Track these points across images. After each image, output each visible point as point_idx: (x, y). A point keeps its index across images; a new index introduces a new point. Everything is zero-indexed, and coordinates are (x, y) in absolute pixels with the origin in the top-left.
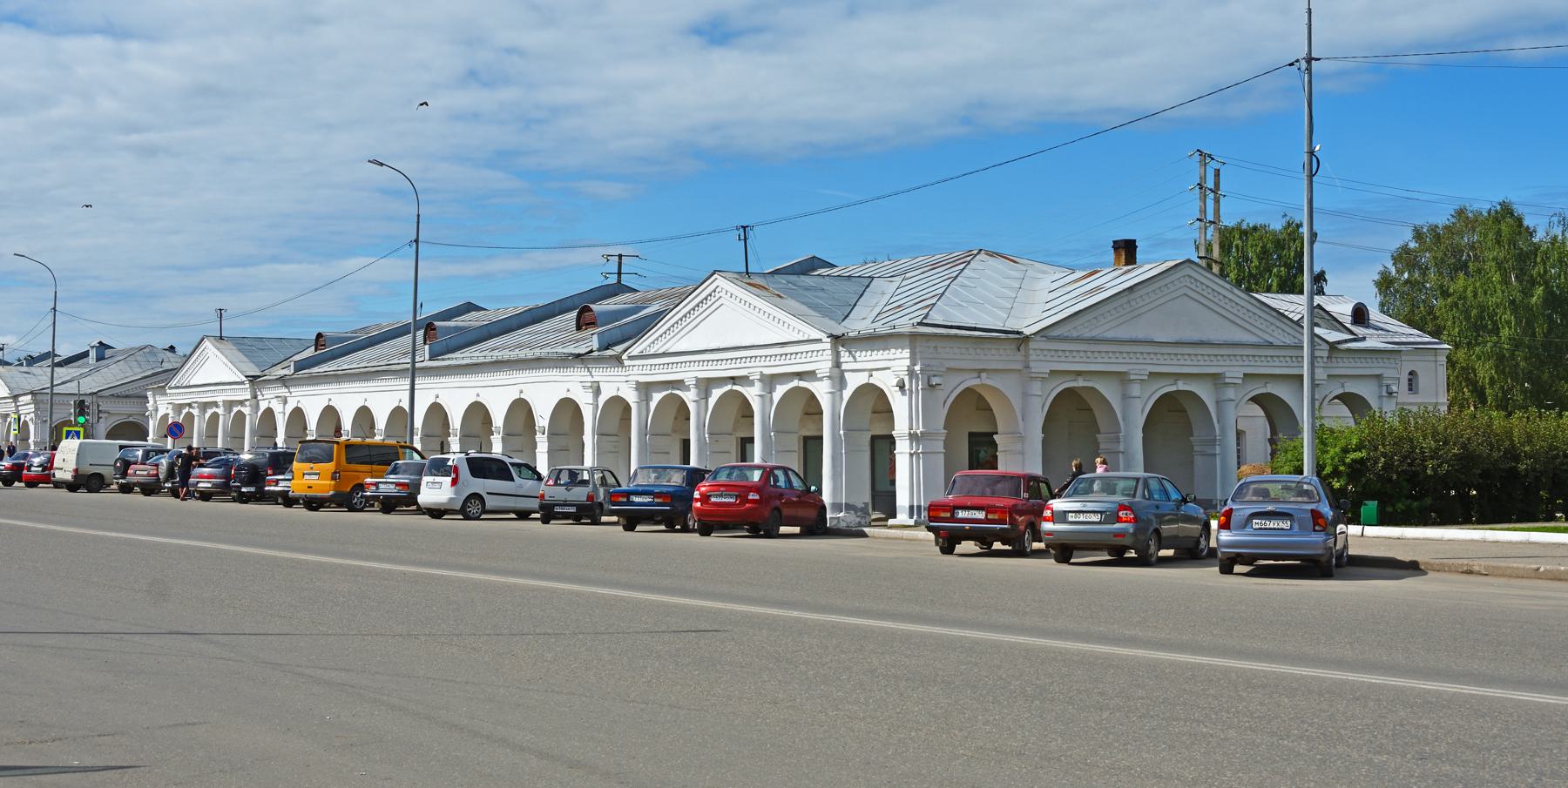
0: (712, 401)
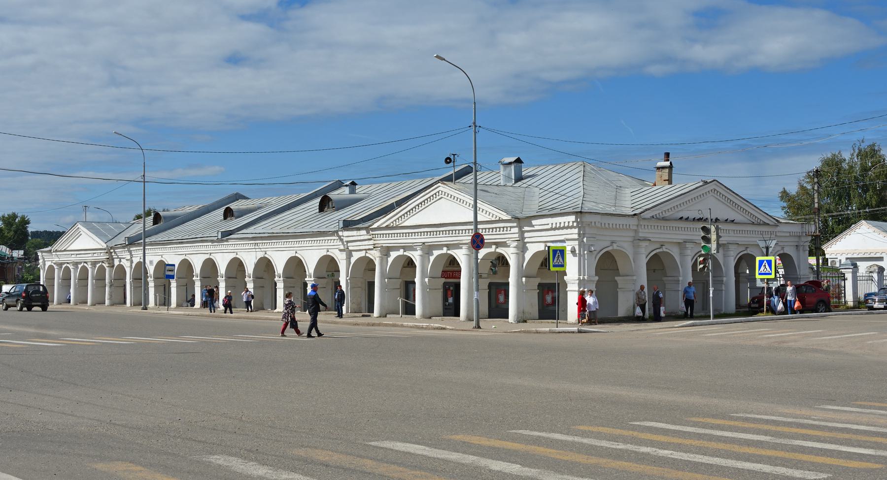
0: (390, 260)
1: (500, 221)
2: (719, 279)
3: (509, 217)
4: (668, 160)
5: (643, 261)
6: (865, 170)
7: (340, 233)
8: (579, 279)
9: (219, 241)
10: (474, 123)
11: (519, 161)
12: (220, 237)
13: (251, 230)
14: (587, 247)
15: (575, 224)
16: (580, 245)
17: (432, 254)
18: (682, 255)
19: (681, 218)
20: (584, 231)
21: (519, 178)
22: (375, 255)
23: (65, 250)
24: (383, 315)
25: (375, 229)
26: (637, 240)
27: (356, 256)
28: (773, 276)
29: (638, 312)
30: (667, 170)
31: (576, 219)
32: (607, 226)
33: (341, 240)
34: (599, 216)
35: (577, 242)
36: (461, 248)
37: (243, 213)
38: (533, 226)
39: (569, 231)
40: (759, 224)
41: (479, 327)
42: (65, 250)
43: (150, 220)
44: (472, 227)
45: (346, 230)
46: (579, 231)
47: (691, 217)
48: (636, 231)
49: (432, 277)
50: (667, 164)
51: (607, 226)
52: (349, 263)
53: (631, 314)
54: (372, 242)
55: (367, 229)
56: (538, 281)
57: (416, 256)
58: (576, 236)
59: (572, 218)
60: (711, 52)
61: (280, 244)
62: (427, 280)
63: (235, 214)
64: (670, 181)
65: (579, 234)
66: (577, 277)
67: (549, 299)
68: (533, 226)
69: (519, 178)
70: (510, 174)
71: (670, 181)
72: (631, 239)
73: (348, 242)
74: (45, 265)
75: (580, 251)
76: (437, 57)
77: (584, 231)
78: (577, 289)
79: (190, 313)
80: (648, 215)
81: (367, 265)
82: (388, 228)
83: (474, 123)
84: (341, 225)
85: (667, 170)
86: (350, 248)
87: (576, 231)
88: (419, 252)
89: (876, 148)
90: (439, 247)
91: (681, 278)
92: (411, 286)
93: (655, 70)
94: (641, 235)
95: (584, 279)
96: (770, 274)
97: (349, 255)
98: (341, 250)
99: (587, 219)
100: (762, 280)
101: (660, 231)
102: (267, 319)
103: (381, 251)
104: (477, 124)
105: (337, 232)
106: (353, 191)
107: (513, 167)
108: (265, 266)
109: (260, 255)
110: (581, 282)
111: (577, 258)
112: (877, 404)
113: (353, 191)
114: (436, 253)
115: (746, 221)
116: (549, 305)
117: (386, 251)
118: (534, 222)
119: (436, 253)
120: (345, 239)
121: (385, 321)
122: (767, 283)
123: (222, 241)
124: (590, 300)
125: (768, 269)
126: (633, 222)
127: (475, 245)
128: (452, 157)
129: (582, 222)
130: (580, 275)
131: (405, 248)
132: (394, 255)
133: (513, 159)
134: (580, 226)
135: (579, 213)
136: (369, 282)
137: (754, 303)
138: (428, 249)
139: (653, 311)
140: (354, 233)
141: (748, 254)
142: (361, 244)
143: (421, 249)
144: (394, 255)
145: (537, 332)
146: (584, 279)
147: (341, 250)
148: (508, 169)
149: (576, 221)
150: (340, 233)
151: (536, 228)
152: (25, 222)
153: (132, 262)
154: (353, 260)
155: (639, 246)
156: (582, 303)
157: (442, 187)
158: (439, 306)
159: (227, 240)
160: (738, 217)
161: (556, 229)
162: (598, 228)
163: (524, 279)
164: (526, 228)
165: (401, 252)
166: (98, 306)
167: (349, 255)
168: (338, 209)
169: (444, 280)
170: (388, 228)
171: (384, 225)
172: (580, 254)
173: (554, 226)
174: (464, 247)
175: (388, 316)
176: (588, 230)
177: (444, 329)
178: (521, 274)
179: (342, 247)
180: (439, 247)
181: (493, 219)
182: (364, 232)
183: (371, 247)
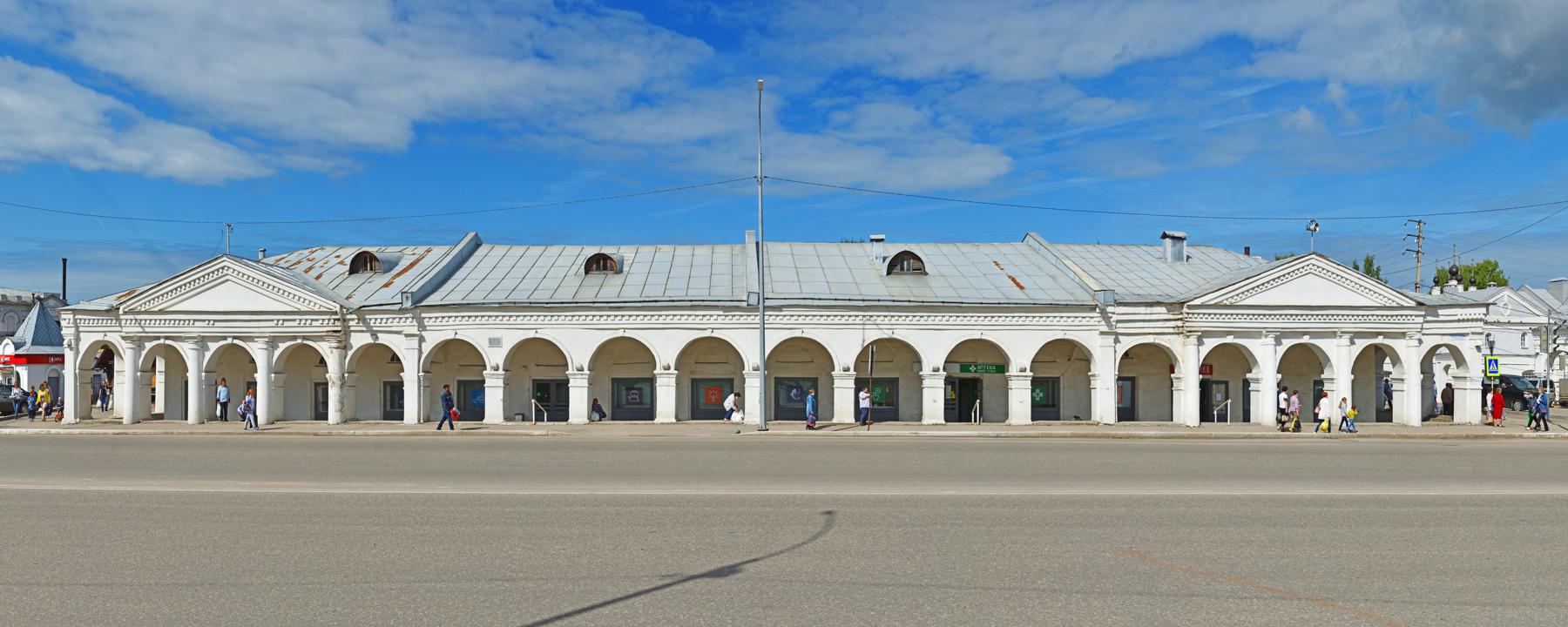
1: (1402, 308)
23: (161, 312)
25: (1190, 307)
27: (1127, 343)
42: (161, 312)
43: (941, 119)
57: (257, 351)
61: (581, 317)
74: (78, 339)
76: (65, 261)
82: (1216, 306)
92: (279, 412)
93: (87, 164)
98: (1102, 333)
116: (550, 399)
118: (1440, 312)
121: (352, 430)
131: (305, 338)
136: (317, 385)
138: (202, 342)
147: (1102, 333)
150: (1110, 309)
152: (1496, 265)
153: (345, 347)
165: (229, 341)
170: (1216, 306)
178: (270, 370)
179: (1106, 329)
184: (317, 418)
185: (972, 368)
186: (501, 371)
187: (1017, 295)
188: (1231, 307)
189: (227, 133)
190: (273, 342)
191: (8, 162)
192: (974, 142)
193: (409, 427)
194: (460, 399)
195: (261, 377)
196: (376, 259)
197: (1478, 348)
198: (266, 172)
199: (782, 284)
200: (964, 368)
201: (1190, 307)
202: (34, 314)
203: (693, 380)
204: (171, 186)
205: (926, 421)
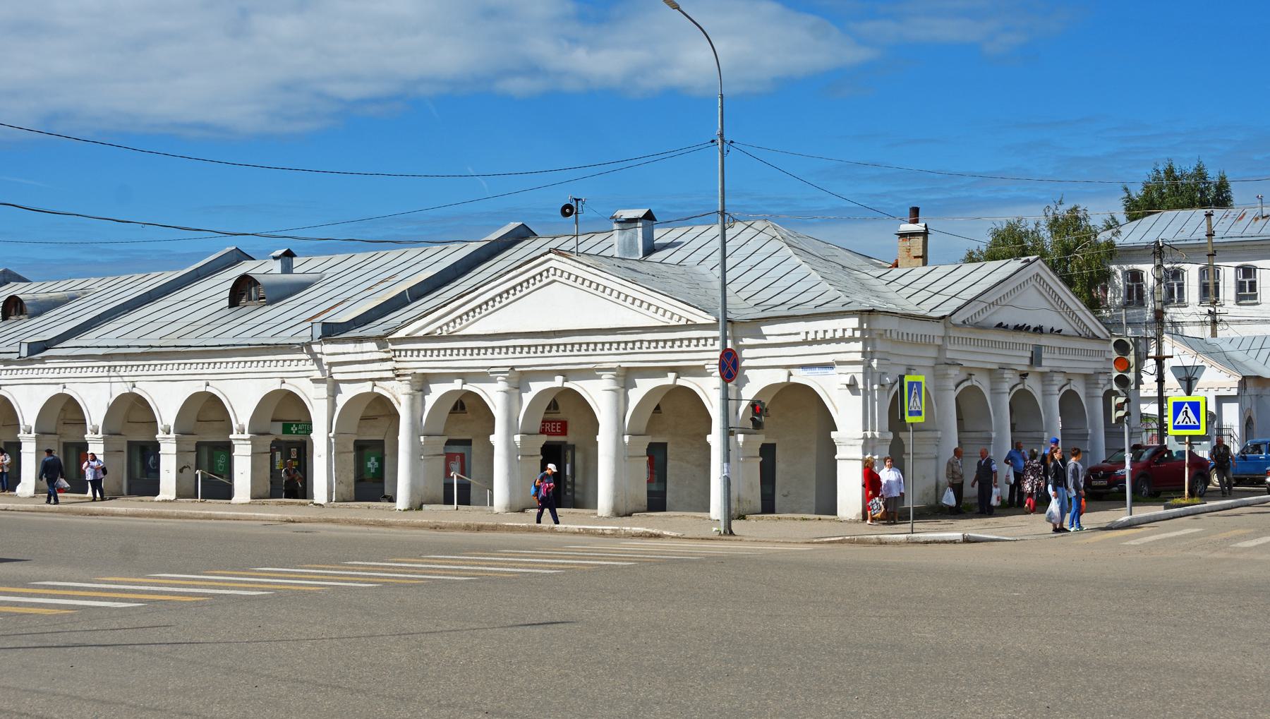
0: (430, 400)
2: (1035, 435)
3: (711, 319)
4: (916, 222)
5: (1056, 400)
6: (1067, 250)
7: (316, 348)
8: (865, 438)
9: (21, 361)
10: (722, 135)
11: (649, 216)
12: (24, 352)
13: (89, 338)
14: (877, 376)
15: (858, 334)
16: (865, 374)
17: (528, 389)
18: (995, 392)
19: (1000, 325)
20: (873, 346)
21: (650, 249)
22: (399, 393)
24: (416, 506)
25: (395, 341)
26: (942, 365)
27: (348, 393)
28: (1202, 432)
29: (949, 499)
30: (921, 239)
31: (861, 323)
32: (894, 335)
33: (318, 361)
34: (896, 319)
35: (860, 368)
36: (599, 377)
37: (43, 308)
38: (764, 337)
39: (843, 346)
40: (1087, 338)
41: (731, 533)
44: (717, 333)
45: (327, 342)
46: (865, 346)
47: (1012, 324)
48: (940, 348)
49: (525, 433)
50: (919, 227)
51: (894, 335)
52: (333, 405)
53: (933, 502)
54: (389, 365)
55: (381, 340)
56: (648, 440)
57: (494, 395)
58: (859, 357)
59: (853, 322)
60: (603, 61)
61: (170, 368)
62: (517, 438)
63: (29, 309)
64: (924, 259)
65: (864, 353)
66: (861, 435)
67: (372, 464)
68: (764, 337)
69: (650, 249)
70: (632, 243)
71: (924, 259)
72: (931, 363)
73: (331, 365)
75: (865, 384)
77: (873, 346)
78: (860, 456)
79: (10, 506)
80: (958, 319)
81: (378, 410)
82: (428, 338)
83: (722, 135)
84: (318, 332)
85: (921, 239)
86: (336, 377)
87: (859, 346)
88: (501, 385)
89: (1081, 215)
90: (548, 375)
91: (994, 435)
93: (518, 86)
94: (949, 355)
95: (873, 437)
96: (1198, 427)
97: (334, 389)
98: (315, 381)
99: (881, 323)
100: (1178, 438)
101: (972, 349)
102: (209, 517)
103: (411, 384)
104: (727, 138)
105: (308, 345)
106: (287, 269)
107: (640, 224)
108: (132, 410)
109: (120, 389)
110: (868, 444)
111: (860, 399)
112: (168, 598)
113: (287, 269)
114: (537, 387)
115: (1072, 332)
117: (422, 383)
118: (766, 329)
119: (537, 387)
120: (326, 359)
121: (417, 518)
122: (1190, 445)
123: (32, 361)
124: (887, 475)
125: (1193, 418)
126: (937, 330)
127: (726, 372)
128: (574, 204)
129: (870, 330)
130: (865, 430)
131: (465, 377)
132: (438, 390)
133: (640, 213)
134: (867, 337)
135: (867, 314)
137: (1096, 478)
138: (519, 380)
139: (973, 496)
140: (350, 347)
141: (973, 387)
142: (362, 368)
143: (507, 380)
144: (438, 390)
145: (881, 543)
146: (873, 437)
147: (315, 381)
148: (628, 233)
149: (860, 328)
150: (316, 348)
151: (770, 340)
154: (341, 401)
155: (945, 376)
156: (871, 482)
157: (556, 262)
158: (641, 493)
159: (42, 360)
160: (1066, 329)
161: (815, 342)
162: (892, 341)
163: (422, 439)
164: (747, 341)
166: (414, 513)
167: (334, 389)
168: (271, 303)
169: (544, 439)
170: (428, 338)
171: (421, 333)
172: (865, 390)
173: (811, 337)
174: (606, 375)
175: (425, 507)
176: (880, 346)
177: (658, 536)
179: (318, 375)
180: (548, 375)
181: (673, 323)
182: (372, 346)
183: (390, 374)
184: (819, 511)
185: (294, 429)
186: (172, 435)
187: (376, 329)
188: (450, 338)
189: (448, 471)
190: (519, 380)
191: (375, 100)
192: (1241, 363)
193: (25, 499)
194: (210, 472)
195: (320, 439)
196: (256, 283)
197: (852, 386)
198: (854, 55)
199: (784, 373)
200: (286, 429)
201: (395, 341)
202: (994, 502)
203: (65, 444)
204: (675, 102)
205: (234, 500)
